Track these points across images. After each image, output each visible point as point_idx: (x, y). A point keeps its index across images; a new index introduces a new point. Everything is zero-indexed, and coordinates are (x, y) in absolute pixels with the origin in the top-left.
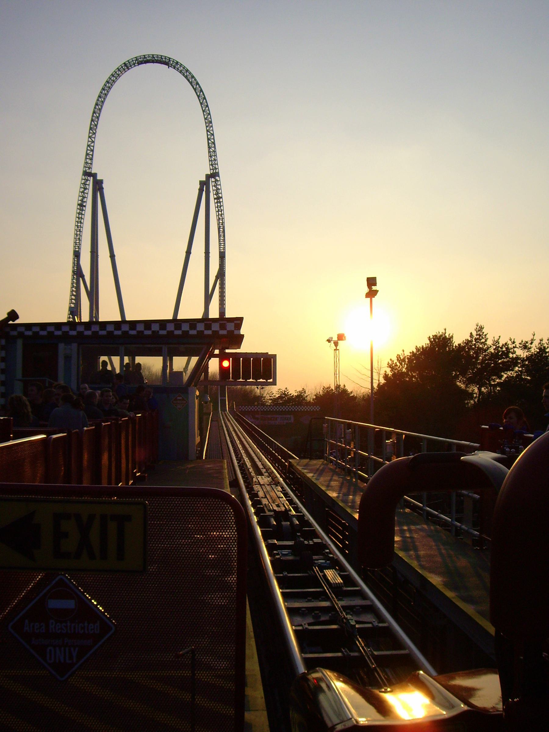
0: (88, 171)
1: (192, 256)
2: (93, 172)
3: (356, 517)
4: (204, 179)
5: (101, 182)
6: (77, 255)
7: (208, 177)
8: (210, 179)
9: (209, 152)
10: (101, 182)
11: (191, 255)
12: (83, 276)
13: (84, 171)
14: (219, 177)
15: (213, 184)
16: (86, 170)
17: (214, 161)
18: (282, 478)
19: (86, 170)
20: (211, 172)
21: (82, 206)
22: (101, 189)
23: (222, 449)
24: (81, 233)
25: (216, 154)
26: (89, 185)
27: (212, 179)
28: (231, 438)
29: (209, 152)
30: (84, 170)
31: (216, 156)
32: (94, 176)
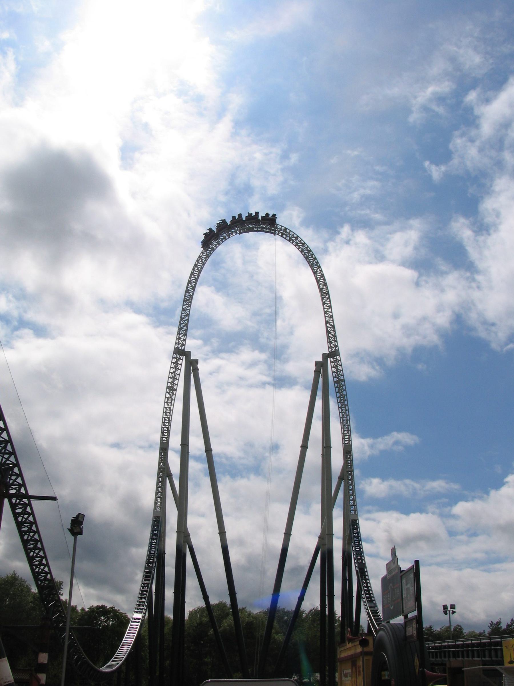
0: (180, 348)
1: (300, 443)
2: (186, 350)
3: (27, 517)
4: (320, 359)
5: (196, 361)
6: (164, 448)
7: (326, 357)
8: (329, 359)
9: (328, 337)
10: (196, 361)
11: (301, 444)
12: (170, 475)
13: (175, 348)
14: (339, 356)
15: (333, 364)
16: (178, 347)
17: (334, 348)
18: (334, 677)
19: (178, 347)
20: (330, 351)
21: (171, 390)
22: (196, 370)
23: (352, 683)
24: (165, 411)
25: (336, 339)
26: (181, 365)
27: (331, 359)
28: (358, 559)
29: (327, 337)
30: (176, 347)
31: (336, 341)
32: (187, 354)
